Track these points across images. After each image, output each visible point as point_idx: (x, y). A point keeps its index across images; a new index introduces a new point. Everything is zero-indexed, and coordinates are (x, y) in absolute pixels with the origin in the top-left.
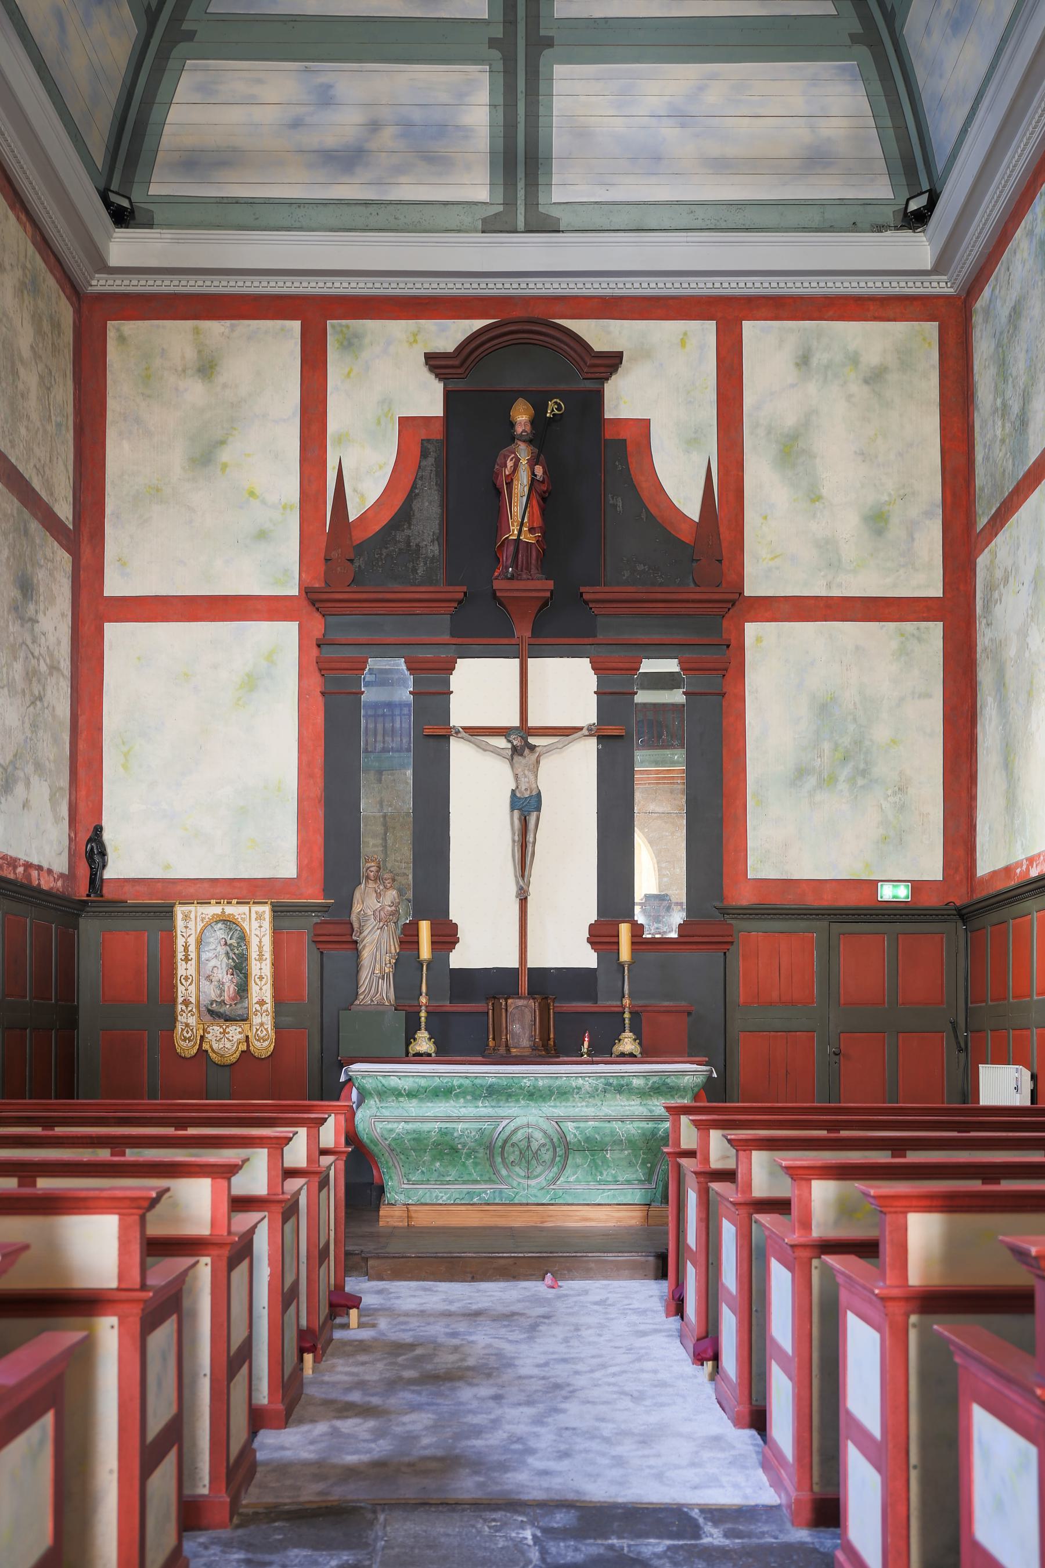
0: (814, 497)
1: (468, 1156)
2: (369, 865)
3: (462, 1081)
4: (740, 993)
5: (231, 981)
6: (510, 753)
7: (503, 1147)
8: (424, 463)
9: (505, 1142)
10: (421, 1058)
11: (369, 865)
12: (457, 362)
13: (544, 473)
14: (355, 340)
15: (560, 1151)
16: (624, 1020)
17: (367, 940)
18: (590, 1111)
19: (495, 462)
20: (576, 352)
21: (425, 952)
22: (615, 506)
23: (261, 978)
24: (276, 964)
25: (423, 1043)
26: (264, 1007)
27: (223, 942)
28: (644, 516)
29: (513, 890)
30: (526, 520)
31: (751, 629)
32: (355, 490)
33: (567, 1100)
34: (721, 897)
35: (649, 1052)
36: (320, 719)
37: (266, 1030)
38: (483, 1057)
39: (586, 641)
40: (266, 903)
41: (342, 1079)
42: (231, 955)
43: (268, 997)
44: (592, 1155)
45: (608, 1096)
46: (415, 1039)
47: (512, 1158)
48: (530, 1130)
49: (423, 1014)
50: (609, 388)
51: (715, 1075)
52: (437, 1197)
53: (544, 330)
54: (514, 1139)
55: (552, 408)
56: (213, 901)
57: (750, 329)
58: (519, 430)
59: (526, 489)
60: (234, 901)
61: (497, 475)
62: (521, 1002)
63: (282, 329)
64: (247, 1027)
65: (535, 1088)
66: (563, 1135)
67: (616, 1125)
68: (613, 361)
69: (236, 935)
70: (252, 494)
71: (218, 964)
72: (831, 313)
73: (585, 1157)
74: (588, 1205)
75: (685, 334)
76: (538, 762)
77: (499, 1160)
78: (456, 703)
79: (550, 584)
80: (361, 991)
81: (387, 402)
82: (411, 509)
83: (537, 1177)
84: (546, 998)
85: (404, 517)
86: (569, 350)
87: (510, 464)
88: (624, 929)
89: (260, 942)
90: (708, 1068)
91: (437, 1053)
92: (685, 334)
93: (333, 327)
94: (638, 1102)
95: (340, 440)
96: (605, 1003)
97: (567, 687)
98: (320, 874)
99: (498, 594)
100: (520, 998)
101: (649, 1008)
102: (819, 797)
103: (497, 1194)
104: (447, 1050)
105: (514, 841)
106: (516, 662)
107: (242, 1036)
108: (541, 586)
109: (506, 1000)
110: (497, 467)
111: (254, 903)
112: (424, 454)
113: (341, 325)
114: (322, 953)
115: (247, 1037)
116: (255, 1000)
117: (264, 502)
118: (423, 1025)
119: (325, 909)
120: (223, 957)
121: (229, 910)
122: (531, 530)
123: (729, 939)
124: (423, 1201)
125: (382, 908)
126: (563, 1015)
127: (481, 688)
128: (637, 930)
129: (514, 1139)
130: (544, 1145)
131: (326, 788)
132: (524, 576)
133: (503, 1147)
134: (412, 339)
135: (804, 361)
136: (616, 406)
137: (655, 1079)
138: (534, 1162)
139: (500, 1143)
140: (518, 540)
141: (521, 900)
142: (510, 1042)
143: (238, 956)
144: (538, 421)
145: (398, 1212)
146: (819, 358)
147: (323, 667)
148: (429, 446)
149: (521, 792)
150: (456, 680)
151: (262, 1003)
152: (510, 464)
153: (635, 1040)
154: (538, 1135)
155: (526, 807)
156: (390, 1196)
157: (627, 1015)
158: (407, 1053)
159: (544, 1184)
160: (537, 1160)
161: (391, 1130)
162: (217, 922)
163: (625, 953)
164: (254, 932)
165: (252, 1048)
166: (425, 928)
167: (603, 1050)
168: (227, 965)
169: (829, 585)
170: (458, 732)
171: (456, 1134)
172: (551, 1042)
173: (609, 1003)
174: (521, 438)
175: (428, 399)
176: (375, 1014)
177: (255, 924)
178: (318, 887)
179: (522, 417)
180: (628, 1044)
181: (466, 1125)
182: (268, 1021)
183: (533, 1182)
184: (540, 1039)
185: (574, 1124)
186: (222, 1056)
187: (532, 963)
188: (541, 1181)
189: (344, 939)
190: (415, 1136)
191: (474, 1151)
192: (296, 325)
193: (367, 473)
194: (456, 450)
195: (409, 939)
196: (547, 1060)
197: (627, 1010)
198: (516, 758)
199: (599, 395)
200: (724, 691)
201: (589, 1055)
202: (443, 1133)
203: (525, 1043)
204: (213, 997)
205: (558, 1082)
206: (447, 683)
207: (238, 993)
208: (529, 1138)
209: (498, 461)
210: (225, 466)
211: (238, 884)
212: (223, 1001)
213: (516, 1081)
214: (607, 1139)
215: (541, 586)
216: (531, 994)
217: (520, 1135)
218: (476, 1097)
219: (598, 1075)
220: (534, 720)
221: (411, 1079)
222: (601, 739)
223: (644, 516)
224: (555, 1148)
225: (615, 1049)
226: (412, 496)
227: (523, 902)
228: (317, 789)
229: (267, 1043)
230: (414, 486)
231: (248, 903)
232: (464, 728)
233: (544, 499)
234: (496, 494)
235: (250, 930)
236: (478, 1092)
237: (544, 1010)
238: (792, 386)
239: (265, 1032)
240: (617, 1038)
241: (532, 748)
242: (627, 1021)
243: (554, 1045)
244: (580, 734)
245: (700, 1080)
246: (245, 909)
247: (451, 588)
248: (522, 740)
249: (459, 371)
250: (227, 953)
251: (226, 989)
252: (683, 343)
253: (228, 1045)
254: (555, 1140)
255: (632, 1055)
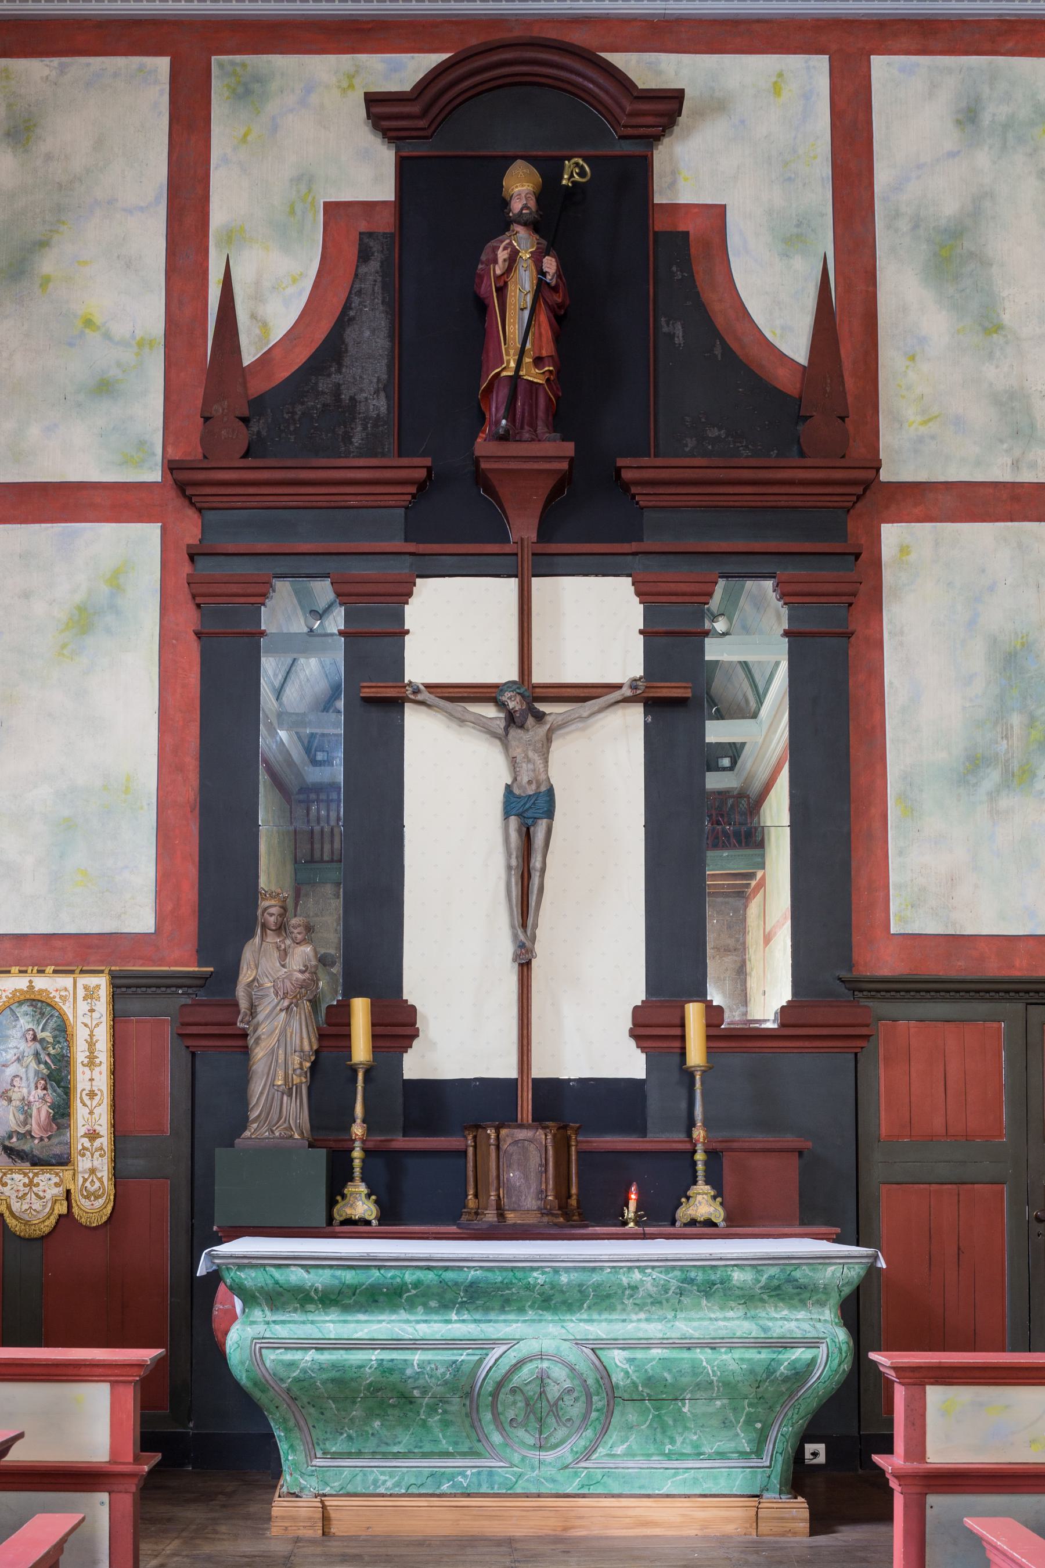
0: (990, 325)
1: (432, 1409)
2: (266, 903)
3: (420, 1274)
4: (884, 1121)
5: (43, 1099)
6: (502, 724)
7: (495, 1394)
8: (363, 269)
9: (500, 1385)
10: (355, 1228)
11: (266, 903)
12: (415, 109)
13: (558, 275)
14: (256, 86)
15: (598, 1402)
16: (695, 1163)
17: (263, 1030)
18: (654, 1329)
19: (478, 261)
20: (607, 92)
21: (361, 1050)
22: (671, 336)
23: (92, 1095)
24: (116, 1072)
25: (361, 1204)
26: (97, 1143)
27: (30, 1037)
28: (718, 351)
29: (506, 948)
30: (528, 346)
31: (892, 536)
32: (253, 316)
33: (611, 1309)
34: (848, 962)
35: (740, 1220)
36: (193, 678)
37: (100, 1180)
38: (459, 1226)
39: (626, 548)
40: (102, 972)
41: (202, 1269)
42: (44, 1057)
43: (104, 1127)
44: (657, 1409)
45: (685, 1300)
46: (344, 1197)
47: (511, 1414)
48: (545, 1365)
49: (357, 1154)
50: (662, 156)
51: (882, 1264)
52: (375, 1482)
53: (556, 58)
54: (516, 1380)
55: (571, 174)
56: (15, 969)
57: (883, 68)
58: (516, 206)
59: (529, 299)
60: (50, 969)
61: (481, 277)
62: (522, 1134)
63: (141, 68)
64: (68, 1175)
65: (553, 1287)
66: (604, 1373)
67: (702, 1355)
68: (667, 108)
69: (52, 1024)
70: (89, 323)
71: (22, 1072)
72: (1010, 45)
73: (645, 1412)
74: (649, 1496)
75: (780, 75)
76: (549, 740)
77: (487, 1416)
78: (412, 647)
79: (569, 449)
80: (253, 1115)
81: (305, 180)
82: (343, 342)
83: (555, 1446)
84: (565, 1127)
85: (331, 353)
86: (597, 90)
87: (502, 255)
88: (694, 1012)
89: (91, 1035)
90: (869, 1251)
91: (382, 1220)
92: (780, 75)
93: (221, 65)
94: (741, 1313)
95: (233, 236)
96: (660, 1138)
97: (595, 623)
98: (191, 927)
99: (484, 465)
100: (521, 1126)
101: (735, 1145)
102: (1004, 802)
103: (484, 1477)
104: (394, 1217)
105: (509, 868)
106: (513, 583)
107: (59, 1191)
108: (555, 451)
109: (498, 1130)
110: (480, 266)
111: (82, 972)
112: (364, 255)
113: (233, 63)
114: (193, 1054)
115: (68, 1192)
116: (82, 1131)
117: (107, 336)
118: (357, 1172)
119: (202, 982)
120: (30, 1060)
121: (41, 983)
122: (538, 361)
123: (864, 1031)
124: (350, 1489)
125: (289, 977)
126: (605, 1156)
127: (454, 624)
128: (714, 1015)
129: (516, 1380)
130: (570, 1391)
131: (202, 786)
132: (526, 436)
133: (495, 1394)
134: (345, 85)
135: (969, 117)
136: (673, 184)
137: (773, 1271)
138: (551, 1420)
139: (489, 1387)
140: (516, 377)
141: (521, 965)
142: (505, 1201)
143: (54, 1058)
144: (549, 192)
145: (306, 1508)
146: (993, 112)
147: (201, 594)
148: (372, 244)
149: (520, 787)
150: (414, 613)
151: (93, 1135)
152: (502, 255)
153: (714, 1198)
154: (559, 1373)
155: (529, 812)
156: (288, 1480)
157: (700, 1156)
158: (330, 1220)
159: (570, 1459)
160: (557, 1417)
161: (292, 1364)
162: (21, 1003)
163: (696, 1054)
164: (80, 1019)
165: (75, 1210)
166: (360, 1009)
167: (662, 1216)
168: (37, 1073)
169: (1016, 465)
170: (416, 691)
171: (409, 1372)
172: (573, 1202)
173: (664, 1137)
174: (520, 220)
175: (370, 175)
176: (274, 1153)
177: (83, 1007)
178: (190, 947)
179: (520, 187)
180: (702, 1203)
181: (429, 1356)
182: (103, 1166)
183: (549, 1456)
184: (556, 1197)
185: (626, 1354)
186: (27, 1223)
187: (540, 1070)
188: (565, 1453)
189: (228, 1030)
190: (333, 1374)
191: (443, 1400)
192: (162, 64)
193: (276, 291)
194: (414, 256)
195: (333, 1031)
196: (567, 1231)
197: (699, 1147)
198: (514, 732)
199: (643, 167)
200: (851, 628)
201: (637, 1223)
202: (386, 1369)
203: (530, 1202)
204: (13, 1125)
205: (596, 1278)
206: (401, 618)
207: (54, 1119)
208: (542, 1379)
209: (483, 258)
210: (46, 281)
211: (58, 944)
212: (29, 1132)
213: (519, 1275)
214: (685, 1380)
215: (555, 451)
216: (540, 1118)
217: (526, 1372)
218: (445, 1306)
219: (667, 1265)
220: (539, 676)
221: (328, 1272)
222: (653, 705)
223: (718, 351)
224: (589, 1397)
225: (680, 1213)
226: (344, 320)
227: (525, 967)
228: (189, 789)
229: (101, 1201)
230: (347, 307)
231: (72, 972)
232: (429, 687)
233: (560, 319)
234: (479, 313)
235: (75, 1017)
236: (449, 1296)
237: (562, 1146)
238: (952, 155)
239: (97, 1184)
240: (681, 1194)
241: (540, 717)
242: (700, 1167)
243: (583, 1205)
244: (616, 695)
245: (854, 1273)
246: (66, 981)
247: (405, 461)
248: (524, 707)
249: (422, 123)
250: (37, 1055)
251: (34, 1112)
252: (776, 89)
253: (37, 1205)
254: (590, 1382)
255: (709, 1223)
